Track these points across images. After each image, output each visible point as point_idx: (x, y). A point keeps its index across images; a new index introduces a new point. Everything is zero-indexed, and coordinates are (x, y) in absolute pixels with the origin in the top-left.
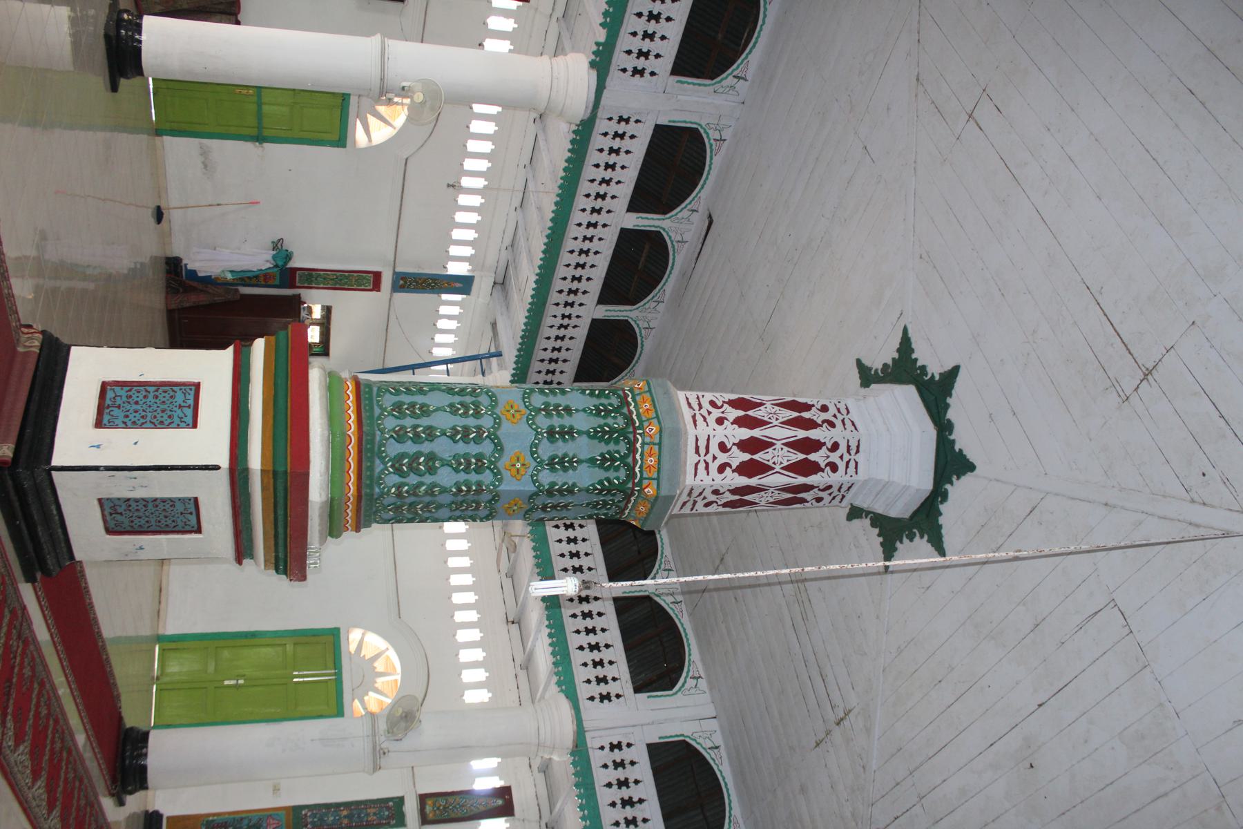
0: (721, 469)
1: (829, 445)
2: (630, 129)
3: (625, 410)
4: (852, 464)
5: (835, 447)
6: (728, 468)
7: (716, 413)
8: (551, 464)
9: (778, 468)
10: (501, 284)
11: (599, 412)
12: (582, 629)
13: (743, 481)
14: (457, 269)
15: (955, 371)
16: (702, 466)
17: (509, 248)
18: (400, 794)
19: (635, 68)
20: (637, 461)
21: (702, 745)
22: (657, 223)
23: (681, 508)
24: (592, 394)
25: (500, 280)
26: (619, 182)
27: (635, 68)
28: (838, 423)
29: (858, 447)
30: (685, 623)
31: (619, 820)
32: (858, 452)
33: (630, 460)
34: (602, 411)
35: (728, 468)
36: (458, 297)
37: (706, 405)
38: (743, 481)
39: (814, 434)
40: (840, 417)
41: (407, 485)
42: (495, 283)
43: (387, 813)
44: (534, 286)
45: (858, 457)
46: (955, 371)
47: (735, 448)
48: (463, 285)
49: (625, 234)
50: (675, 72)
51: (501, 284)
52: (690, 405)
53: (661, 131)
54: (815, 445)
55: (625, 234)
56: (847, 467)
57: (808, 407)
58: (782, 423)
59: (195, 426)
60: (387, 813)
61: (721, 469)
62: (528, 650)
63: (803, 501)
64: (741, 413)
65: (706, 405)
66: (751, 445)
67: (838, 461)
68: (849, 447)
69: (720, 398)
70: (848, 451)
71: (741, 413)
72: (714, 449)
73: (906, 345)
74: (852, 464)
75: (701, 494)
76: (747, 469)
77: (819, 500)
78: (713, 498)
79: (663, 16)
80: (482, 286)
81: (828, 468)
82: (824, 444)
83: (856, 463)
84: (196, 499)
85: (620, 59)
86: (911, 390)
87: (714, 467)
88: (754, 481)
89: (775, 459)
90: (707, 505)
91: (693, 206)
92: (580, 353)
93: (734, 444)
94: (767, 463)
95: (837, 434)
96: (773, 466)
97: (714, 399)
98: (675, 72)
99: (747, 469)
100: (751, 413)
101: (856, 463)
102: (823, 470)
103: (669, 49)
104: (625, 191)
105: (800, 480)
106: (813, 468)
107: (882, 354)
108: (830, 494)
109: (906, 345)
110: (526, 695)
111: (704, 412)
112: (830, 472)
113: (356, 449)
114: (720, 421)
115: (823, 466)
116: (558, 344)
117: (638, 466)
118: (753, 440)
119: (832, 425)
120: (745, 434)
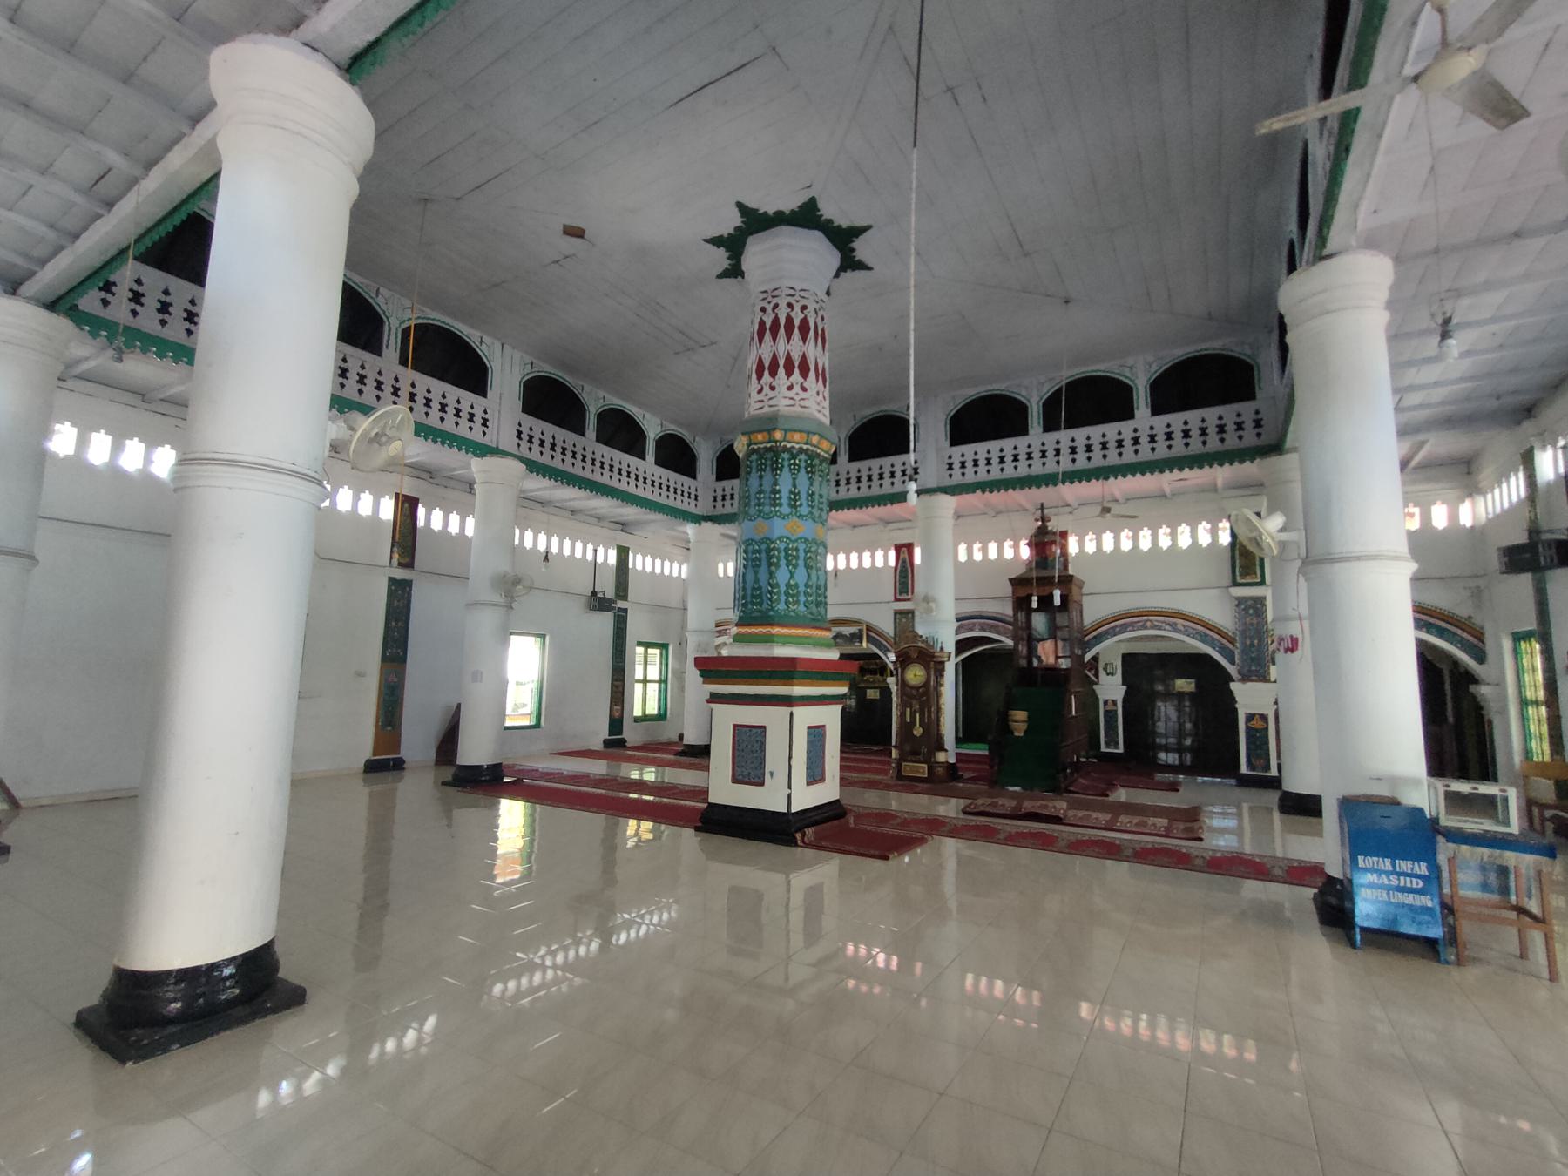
0: (804, 389)
2: (526, 431)
3: (762, 451)
4: (802, 294)
7: (766, 390)
8: (795, 507)
9: (774, 348)
10: (623, 526)
11: (761, 470)
12: (857, 486)
13: (812, 374)
15: (740, 206)
16: (802, 403)
18: (387, 578)
21: (953, 407)
24: (749, 473)
25: (620, 527)
26: (542, 434)
28: (775, 301)
31: (171, 296)
36: (631, 555)
37: (761, 397)
39: (783, 321)
40: (770, 299)
42: (622, 531)
43: (400, 592)
45: (798, 288)
46: (740, 206)
47: (791, 379)
48: (623, 553)
50: (483, 394)
51: (623, 526)
52: (761, 408)
53: (527, 409)
54: (789, 320)
57: (762, 323)
58: (774, 342)
59: (764, 727)
60: (400, 592)
61: (804, 389)
62: (877, 522)
63: (823, 330)
64: (766, 373)
65: (761, 397)
69: (754, 385)
70: (793, 296)
71: (766, 373)
73: (717, 241)
75: (818, 404)
76: (804, 372)
77: (823, 319)
78: (821, 395)
79: (363, 387)
80: (624, 540)
82: (788, 314)
83: (802, 290)
84: (809, 728)
85: (476, 436)
86: (751, 240)
87: (803, 395)
88: (812, 367)
92: (686, 478)
97: (757, 390)
98: (483, 394)
99: (804, 372)
100: (767, 365)
101: (802, 290)
103: (468, 398)
104: (571, 437)
106: (804, 322)
107: (720, 258)
109: (717, 241)
110: (908, 524)
111: (766, 399)
114: (773, 388)
116: (672, 490)
118: (785, 367)
119: (776, 306)
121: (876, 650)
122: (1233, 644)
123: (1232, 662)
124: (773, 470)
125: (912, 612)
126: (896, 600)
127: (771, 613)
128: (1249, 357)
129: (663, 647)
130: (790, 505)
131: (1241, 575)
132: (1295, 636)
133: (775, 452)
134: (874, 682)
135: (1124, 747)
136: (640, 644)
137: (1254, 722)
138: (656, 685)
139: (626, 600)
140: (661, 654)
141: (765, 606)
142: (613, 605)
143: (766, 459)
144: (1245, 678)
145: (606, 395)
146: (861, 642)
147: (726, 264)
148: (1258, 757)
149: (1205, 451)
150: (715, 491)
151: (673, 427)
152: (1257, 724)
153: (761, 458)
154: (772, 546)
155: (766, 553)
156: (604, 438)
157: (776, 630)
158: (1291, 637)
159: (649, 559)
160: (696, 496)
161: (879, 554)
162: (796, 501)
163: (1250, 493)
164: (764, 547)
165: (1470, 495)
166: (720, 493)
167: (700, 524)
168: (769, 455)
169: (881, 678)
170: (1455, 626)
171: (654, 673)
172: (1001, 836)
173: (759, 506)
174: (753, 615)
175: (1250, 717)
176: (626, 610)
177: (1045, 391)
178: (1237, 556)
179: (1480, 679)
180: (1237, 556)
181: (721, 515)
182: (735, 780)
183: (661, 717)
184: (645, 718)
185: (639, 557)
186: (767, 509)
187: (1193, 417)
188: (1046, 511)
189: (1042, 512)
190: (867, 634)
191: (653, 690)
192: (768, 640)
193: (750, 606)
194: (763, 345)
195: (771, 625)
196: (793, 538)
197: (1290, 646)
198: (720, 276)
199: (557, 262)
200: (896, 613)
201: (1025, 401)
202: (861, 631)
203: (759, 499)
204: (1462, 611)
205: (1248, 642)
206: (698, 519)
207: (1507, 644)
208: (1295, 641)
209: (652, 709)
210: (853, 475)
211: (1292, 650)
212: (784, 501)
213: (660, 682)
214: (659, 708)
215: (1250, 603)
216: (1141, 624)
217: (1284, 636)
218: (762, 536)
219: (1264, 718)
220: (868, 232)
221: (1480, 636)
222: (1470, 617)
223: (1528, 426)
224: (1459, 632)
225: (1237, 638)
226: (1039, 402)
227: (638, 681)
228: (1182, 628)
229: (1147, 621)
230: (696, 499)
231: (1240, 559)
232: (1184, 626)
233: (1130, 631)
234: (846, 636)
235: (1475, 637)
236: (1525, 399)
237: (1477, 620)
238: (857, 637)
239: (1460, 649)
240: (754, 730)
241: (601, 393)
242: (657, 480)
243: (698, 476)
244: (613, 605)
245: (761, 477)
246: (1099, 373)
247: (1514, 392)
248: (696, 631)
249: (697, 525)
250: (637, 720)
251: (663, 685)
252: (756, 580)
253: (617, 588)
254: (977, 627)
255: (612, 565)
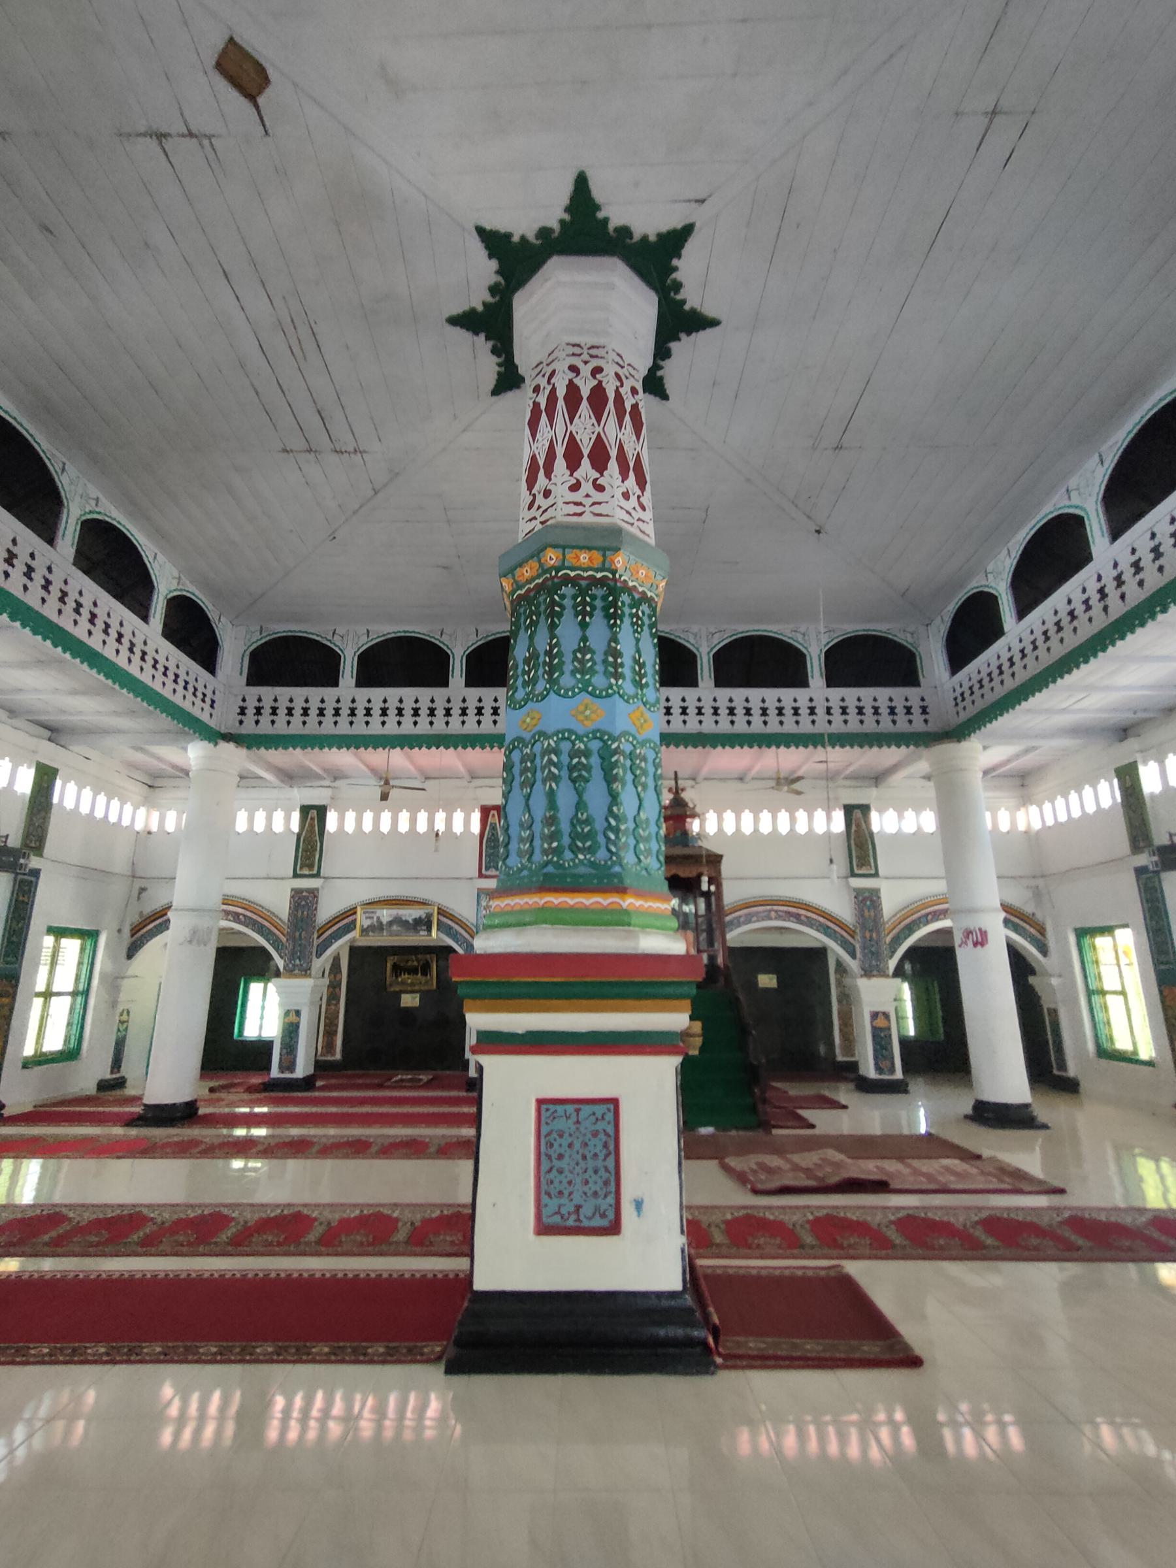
1: (571, 375)
4: (593, 352)
5: (574, 369)
6: (598, 482)
9: (599, 429)
10: (54, 732)
13: (613, 466)
14: (838, 823)
17: (797, 786)
19: (718, 708)
20: (578, 575)
22: (705, 660)
23: (648, 535)
25: (48, 733)
27: (718, 708)
29: (574, 345)
30: (952, 607)
32: (579, 346)
33: (583, 583)
34: (532, 620)
35: (598, 482)
36: (58, 783)
38: (613, 466)
39: (561, 392)
41: (543, 830)
42: (50, 740)
44: (95, 670)
48: (45, 778)
49: (720, 682)
51: (54, 732)
54: (572, 389)
55: (720, 682)
56: (596, 357)
66: (573, 458)
67: (590, 366)
68: (573, 355)
71: (541, 473)
72: (577, 496)
74: (593, 352)
78: (633, 499)
80: (50, 754)
81: (598, 376)
82: (571, 381)
84: (540, 1102)
88: (613, 453)
89: (589, 431)
90: (643, 508)
91: (58, 467)
93: (571, 475)
94: (592, 441)
95: (561, 366)
96: (596, 434)
102: (600, 382)
105: (611, 405)
108: (627, 378)
112: (603, 374)
113: (589, 895)
115: (595, 382)
117: (581, 573)
120: (560, 464)
121: (263, 942)
122: (853, 937)
123: (853, 956)
124: (608, 617)
125: (223, 904)
126: (481, 875)
127: (617, 869)
128: (911, 644)
129: (88, 935)
130: (634, 681)
131: (857, 866)
132: (983, 929)
133: (612, 588)
134: (412, 984)
135: (1058, 1076)
136: (51, 930)
137: (878, 1020)
138: (68, 999)
139: (41, 855)
140: (82, 950)
141: (602, 854)
142: (22, 861)
143: (593, 597)
144: (868, 973)
145: (103, 499)
146: (429, 930)
147: (478, 298)
148: (885, 1058)
149: (877, 731)
150: (244, 700)
151: (192, 589)
152: (881, 1022)
153: (583, 592)
154: (614, 746)
155: (602, 758)
156: (86, 561)
157: (629, 902)
158: (980, 930)
159: (87, 793)
160: (213, 702)
161: (458, 817)
162: (642, 677)
163: (859, 784)
164: (595, 745)
165: (1024, 805)
166: (251, 705)
167: (216, 744)
168: (599, 592)
169: (423, 979)
170: (1026, 922)
171: (65, 979)
172: (432, 1150)
173: (583, 673)
174: (576, 871)
175: (875, 1015)
176: (36, 873)
177: (716, 642)
178: (853, 847)
179: (1037, 969)
180: (853, 847)
181: (266, 736)
182: (544, 1229)
183: (70, 1054)
184: (42, 1059)
185: (72, 787)
186: (599, 680)
187: (866, 694)
188: (680, 782)
189: (676, 783)
190: (438, 919)
191: (61, 1008)
192: (618, 920)
193: (568, 855)
194: (538, 436)
195: (622, 890)
196: (640, 738)
197: (980, 940)
198: (454, 321)
199: (161, 136)
200: (480, 892)
201: (695, 651)
202: (429, 917)
203: (582, 662)
204: (1029, 909)
205: (868, 935)
206: (215, 736)
207: (1072, 939)
208: (984, 934)
209: (54, 1042)
210: (472, 705)
211: (982, 944)
212: (626, 671)
213: (74, 994)
214: (67, 1040)
215: (867, 894)
216: (765, 914)
217: (972, 928)
218: (590, 726)
219: (886, 1016)
220: (709, 331)
221: (1042, 931)
222: (1033, 914)
223: (1132, 744)
224: (1028, 927)
225: (858, 931)
226: (709, 653)
227: (38, 995)
228: (805, 920)
229: (770, 911)
230: (212, 706)
231: (856, 851)
232: (807, 917)
233: (755, 922)
234: (407, 922)
235: (1039, 931)
236: (1127, 717)
237: (1039, 916)
238: (424, 923)
239: (1030, 942)
240: (586, 1110)
241: (94, 492)
242: (162, 661)
243: (219, 672)
244: (22, 861)
245: (584, 625)
246: (770, 634)
247: (1145, 710)
248: (193, 910)
249: (211, 745)
250: (27, 1064)
251: (79, 999)
252: (580, 805)
253: (27, 835)
254: (773, 914)
255: (24, 794)
